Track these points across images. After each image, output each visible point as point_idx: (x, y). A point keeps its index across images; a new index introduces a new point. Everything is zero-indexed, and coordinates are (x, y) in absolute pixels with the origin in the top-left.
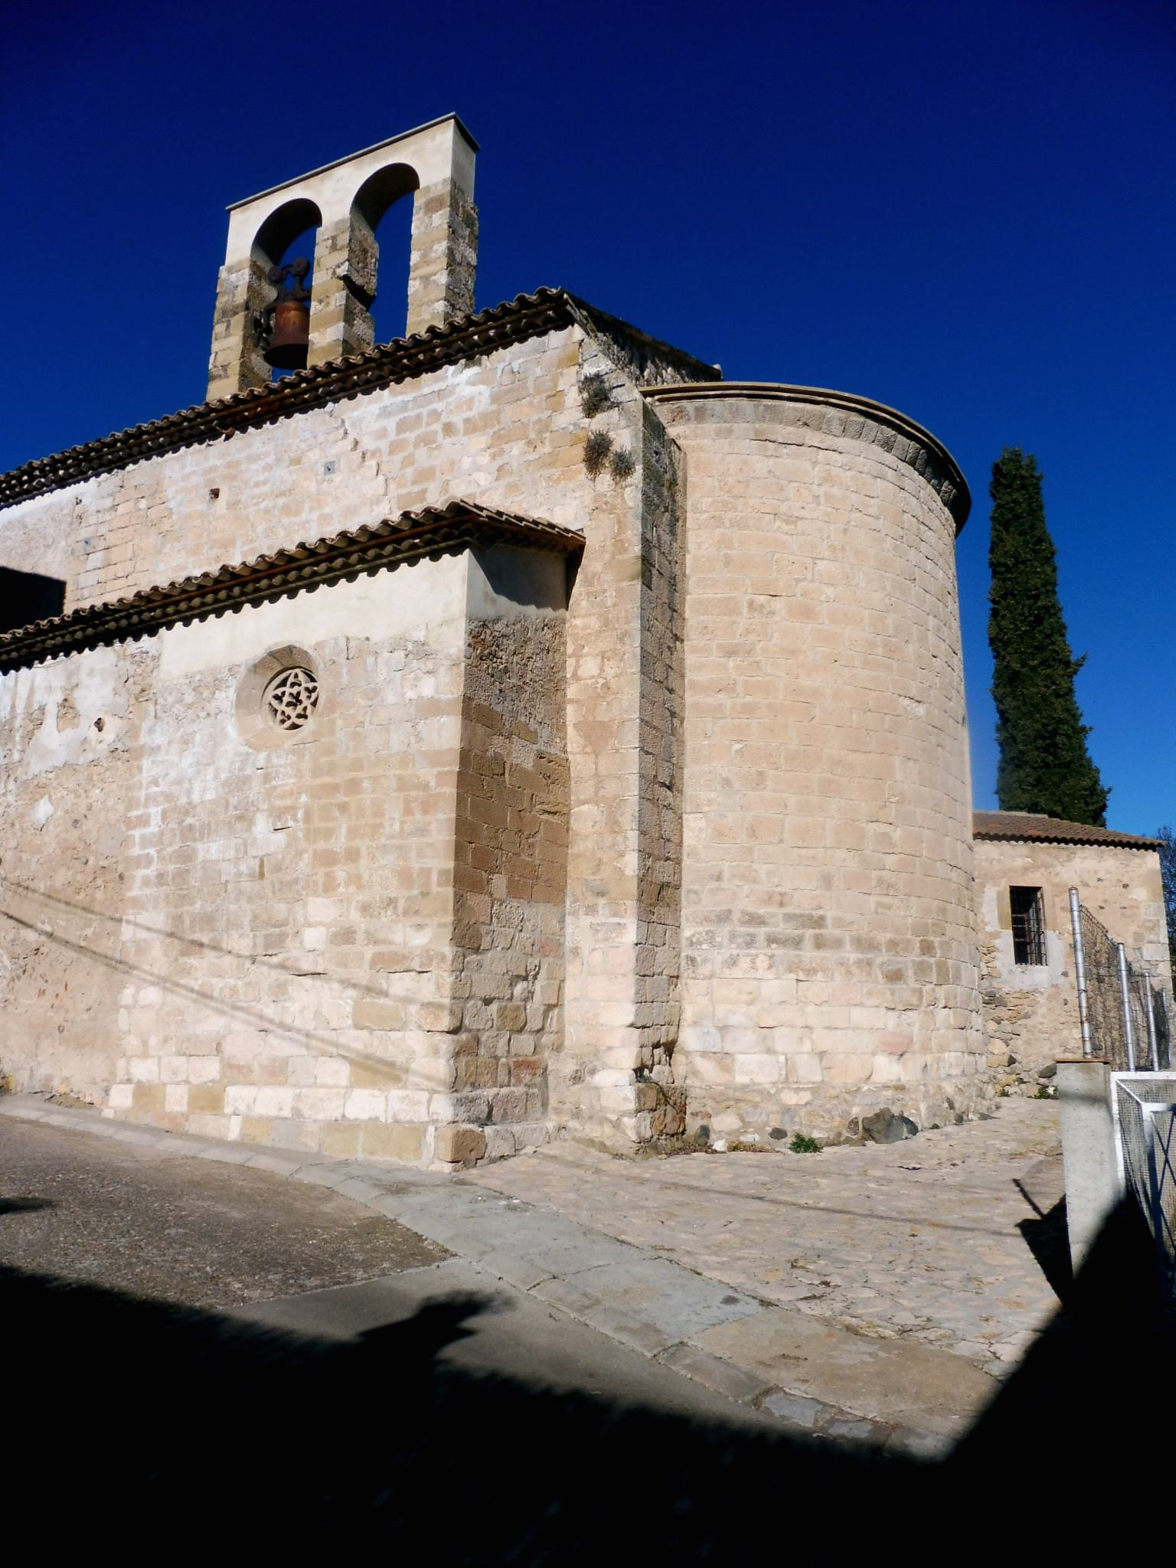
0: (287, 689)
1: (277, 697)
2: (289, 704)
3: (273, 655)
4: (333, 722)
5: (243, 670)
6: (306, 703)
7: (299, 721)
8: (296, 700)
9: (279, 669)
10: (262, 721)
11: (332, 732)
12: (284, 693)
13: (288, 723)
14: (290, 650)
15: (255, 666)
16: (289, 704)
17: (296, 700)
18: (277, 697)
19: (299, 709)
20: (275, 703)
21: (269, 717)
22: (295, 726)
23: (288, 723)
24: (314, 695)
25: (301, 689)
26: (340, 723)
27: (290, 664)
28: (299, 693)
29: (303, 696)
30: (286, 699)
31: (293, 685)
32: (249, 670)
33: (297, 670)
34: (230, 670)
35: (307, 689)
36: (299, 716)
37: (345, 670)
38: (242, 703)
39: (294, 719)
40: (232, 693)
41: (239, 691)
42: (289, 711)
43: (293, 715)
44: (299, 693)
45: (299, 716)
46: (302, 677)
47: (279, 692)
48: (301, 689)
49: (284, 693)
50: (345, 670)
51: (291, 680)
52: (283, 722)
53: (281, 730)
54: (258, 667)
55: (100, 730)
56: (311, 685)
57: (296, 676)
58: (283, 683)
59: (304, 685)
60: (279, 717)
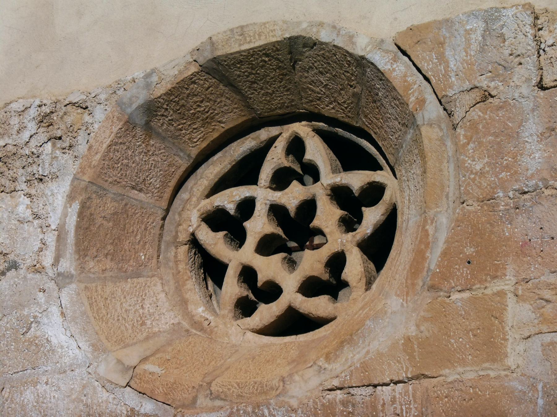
0: (263, 194)
1: (216, 220)
2: (267, 246)
3: (221, 71)
4: (491, 313)
5: (101, 125)
6: (337, 240)
7: (318, 306)
8: (296, 230)
9: (231, 119)
10: (161, 297)
11: (490, 346)
12: (247, 207)
13: (267, 313)
14: (292, 54)
15: (151, 109)
16: (267, 246)
17: (296, 230)
18: (216, 220)
19: (312, 262)
20: (215, 242)
21: (193, 289)
22: (294, 323)
23: (267, 313)
24: (372, 217)
25: (319, 191)
26: (517, 313)
27: (280, 101)
28: (309, 207)
29: (328, 216)
30: (259, 225)
31: (281, 180)
32: (129, 125)
33: (302, 129)
34: (45, 120)
35: (340, 194)
36: (311, 287)
37: (532, 128)
38: (102, 237)
39: (291, 296)
40: (58, 202)
41: (87, 194)
42: (269, 268)
43: (290, 282)
44: (309, 207)
45: (311, 287)
46: (317, 151)
47: (229, 199)
48: (319, 191)
49: (247, 207)
50: (532, 128)
51: (277, 158)
52: (245, 308)
53: (241, 336)
54: (156, 114)
55: (367, 290)
56: (356, 180)
57: (296, 147)
58: (245, 172)
59: (330, 177)
60: (232, 288)
